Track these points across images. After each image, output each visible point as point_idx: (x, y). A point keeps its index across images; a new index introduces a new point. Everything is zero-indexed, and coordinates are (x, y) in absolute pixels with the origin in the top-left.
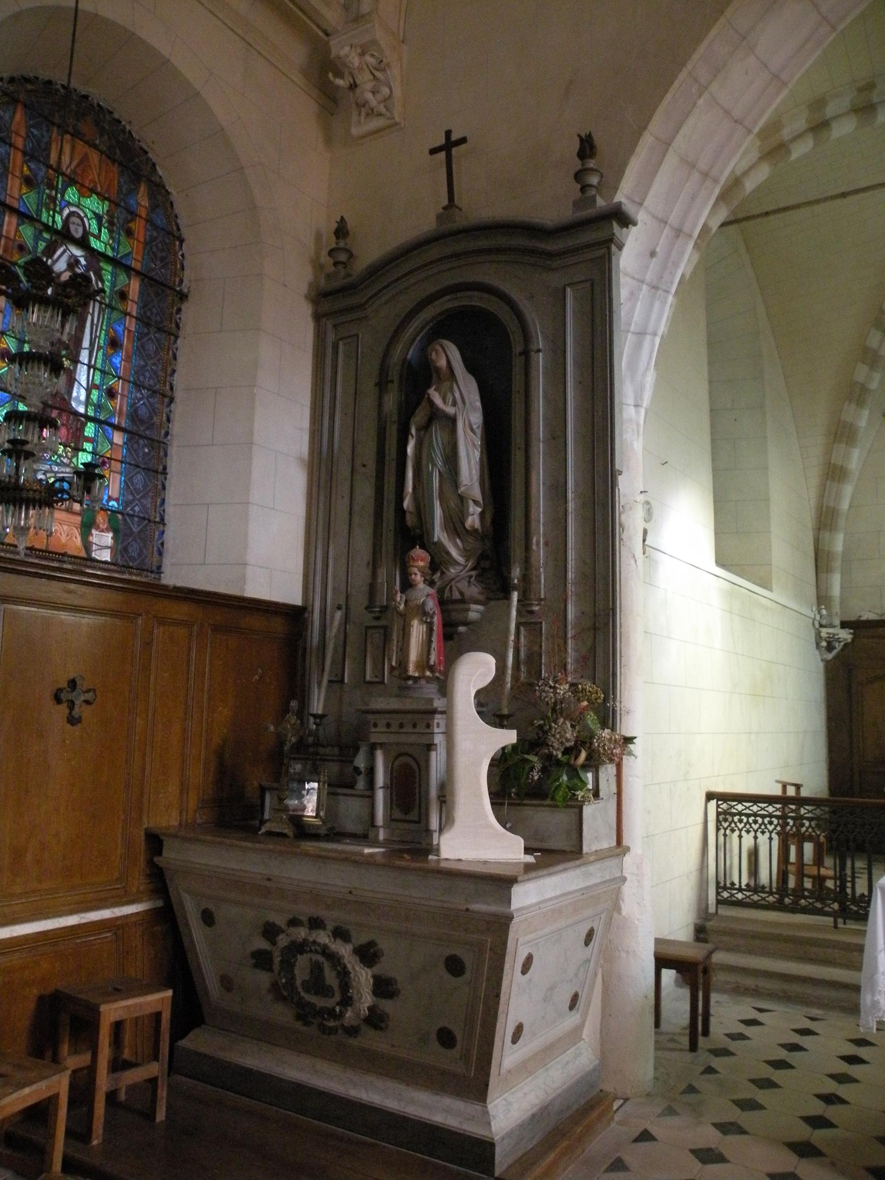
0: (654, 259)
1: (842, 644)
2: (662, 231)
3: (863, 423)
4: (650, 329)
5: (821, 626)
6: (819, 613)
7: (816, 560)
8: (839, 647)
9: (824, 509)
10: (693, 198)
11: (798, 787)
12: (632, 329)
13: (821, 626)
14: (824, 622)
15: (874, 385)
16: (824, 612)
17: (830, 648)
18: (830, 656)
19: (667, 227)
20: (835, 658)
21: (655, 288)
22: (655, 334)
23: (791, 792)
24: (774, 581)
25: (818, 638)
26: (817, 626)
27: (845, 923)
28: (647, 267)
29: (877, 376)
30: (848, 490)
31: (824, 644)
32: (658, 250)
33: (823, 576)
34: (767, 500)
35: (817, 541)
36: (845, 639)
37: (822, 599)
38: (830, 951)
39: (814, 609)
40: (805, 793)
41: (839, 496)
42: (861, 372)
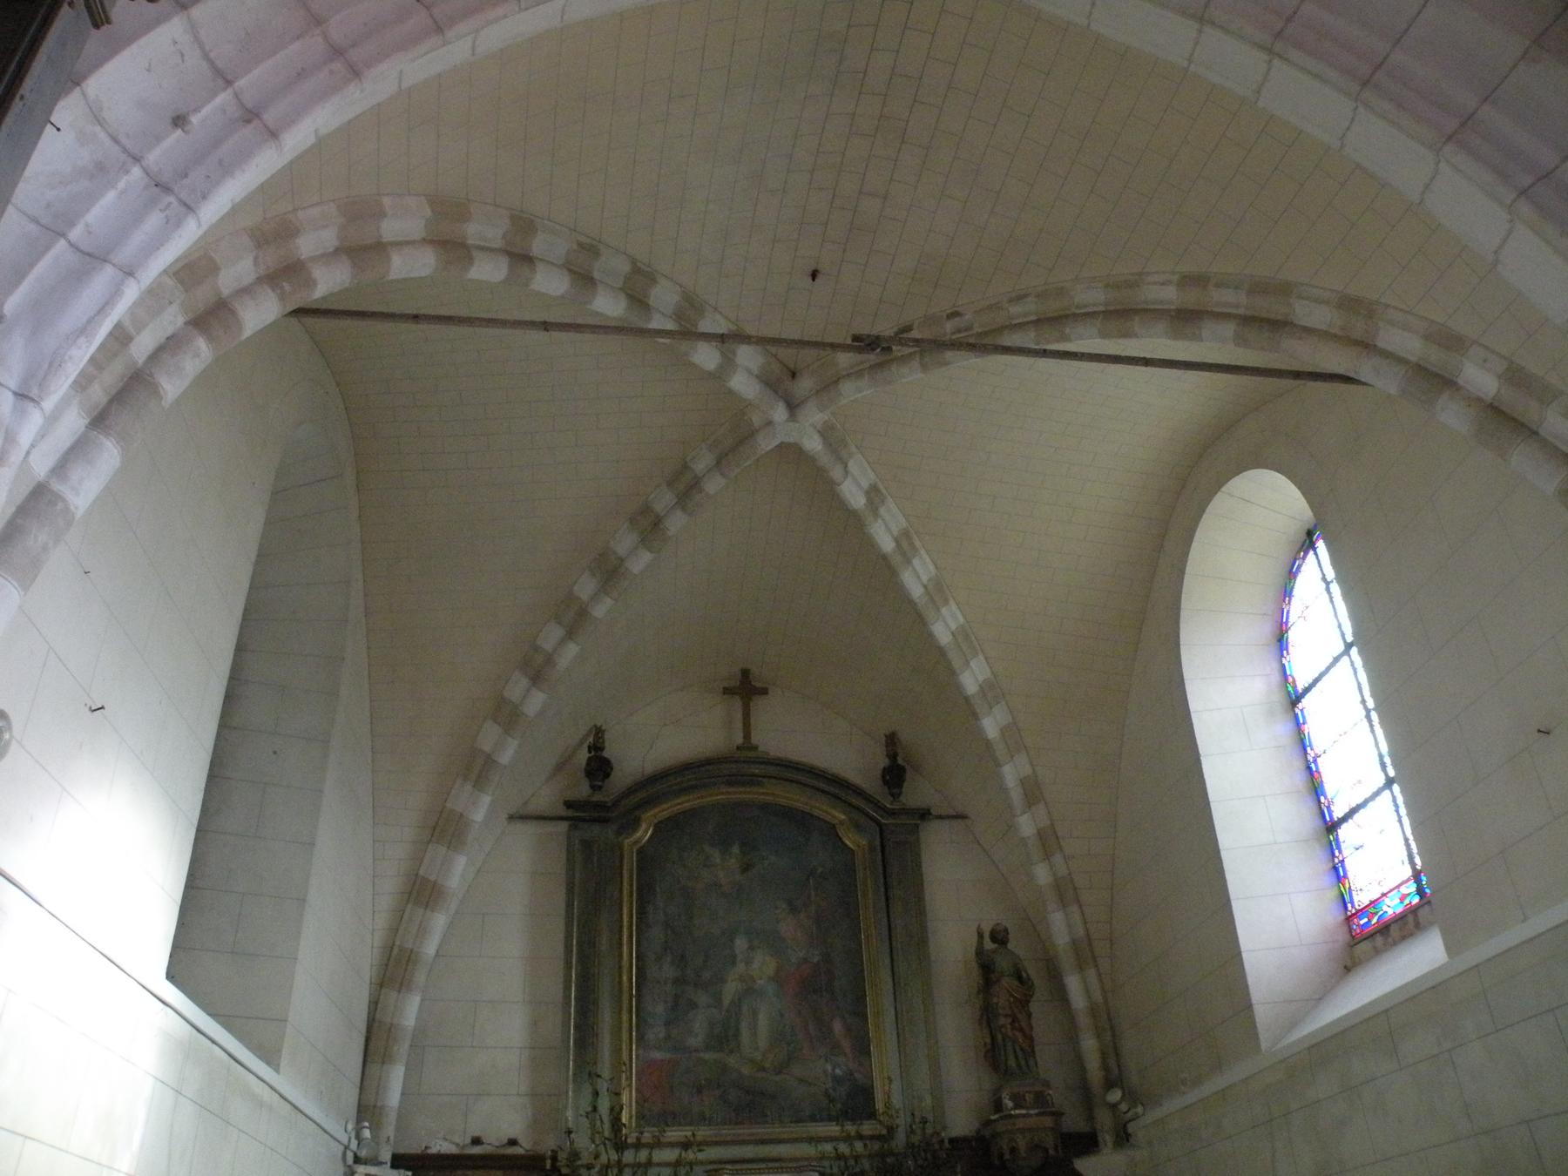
0: (179, 132)
2: (214, 94)
3: (478, 815)
4: (125, 254)
5: (357, 1160)
6: (358, 1137)
7: (368, 1040)
9: (396, 951)
10: (301, 75)
12: (76, 234)
13: (357, 1160)
14: (363, 1153)
15: (505, 758)
16: (367, 1133)
19: (230, 90)
21: (161, 186)
22: (129, 273)
24: (285, 1052)
26: (350, 1156)
28: (158, 139)
29: (512, 745)
30: (439, 921)
32: (195, 119)
33: (373, 1069)
34: (302, 901)
35: (374, 1005)
37: (367, 1111)
39: (350, 1127)
41: (423, 931)
42: (489, 736)
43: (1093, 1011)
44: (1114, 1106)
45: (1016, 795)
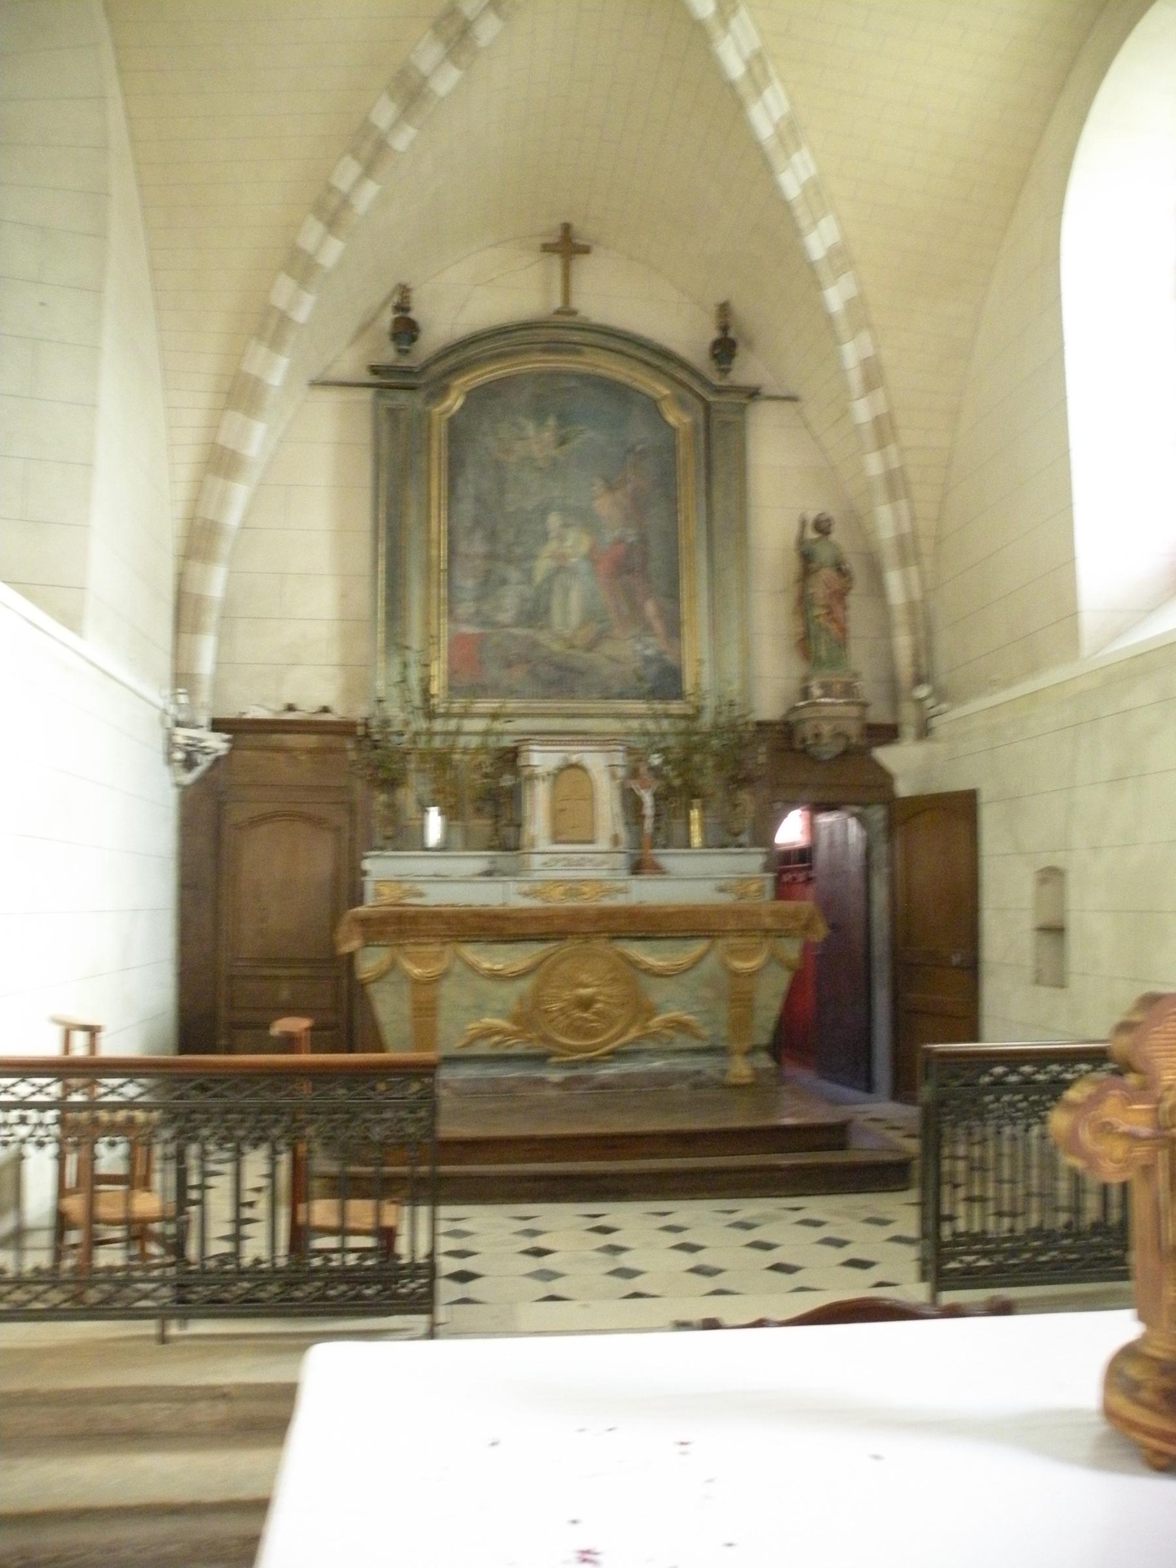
1: (211, 757)
5: (179, 724)
8: (204, 762)
11: (92, 1031)
15: (301, 315)
16: (183, 699)
17: (189, 763)
18: (188, 778)
20: (201, 781)
23: (80, 1049)
25: (171, 744)
26: (170, 724)
27: (165, 1158)
30: (240, 492)
31: (179, 755)
34: (89, 465)
35: (181, 577)
36: (217, 751)
37: (182, 679)
38: (145, 1407)
40: (111, 1048)
41: (224, 502)
43: (911, 607)
44: (920, 701)
45: (855, 378)
